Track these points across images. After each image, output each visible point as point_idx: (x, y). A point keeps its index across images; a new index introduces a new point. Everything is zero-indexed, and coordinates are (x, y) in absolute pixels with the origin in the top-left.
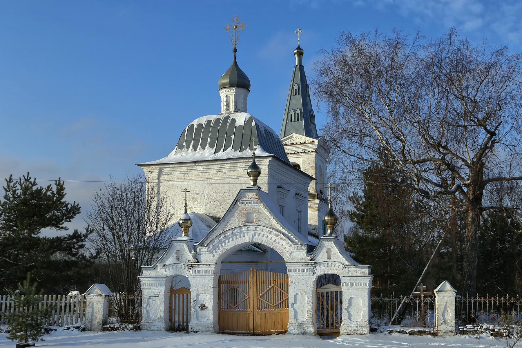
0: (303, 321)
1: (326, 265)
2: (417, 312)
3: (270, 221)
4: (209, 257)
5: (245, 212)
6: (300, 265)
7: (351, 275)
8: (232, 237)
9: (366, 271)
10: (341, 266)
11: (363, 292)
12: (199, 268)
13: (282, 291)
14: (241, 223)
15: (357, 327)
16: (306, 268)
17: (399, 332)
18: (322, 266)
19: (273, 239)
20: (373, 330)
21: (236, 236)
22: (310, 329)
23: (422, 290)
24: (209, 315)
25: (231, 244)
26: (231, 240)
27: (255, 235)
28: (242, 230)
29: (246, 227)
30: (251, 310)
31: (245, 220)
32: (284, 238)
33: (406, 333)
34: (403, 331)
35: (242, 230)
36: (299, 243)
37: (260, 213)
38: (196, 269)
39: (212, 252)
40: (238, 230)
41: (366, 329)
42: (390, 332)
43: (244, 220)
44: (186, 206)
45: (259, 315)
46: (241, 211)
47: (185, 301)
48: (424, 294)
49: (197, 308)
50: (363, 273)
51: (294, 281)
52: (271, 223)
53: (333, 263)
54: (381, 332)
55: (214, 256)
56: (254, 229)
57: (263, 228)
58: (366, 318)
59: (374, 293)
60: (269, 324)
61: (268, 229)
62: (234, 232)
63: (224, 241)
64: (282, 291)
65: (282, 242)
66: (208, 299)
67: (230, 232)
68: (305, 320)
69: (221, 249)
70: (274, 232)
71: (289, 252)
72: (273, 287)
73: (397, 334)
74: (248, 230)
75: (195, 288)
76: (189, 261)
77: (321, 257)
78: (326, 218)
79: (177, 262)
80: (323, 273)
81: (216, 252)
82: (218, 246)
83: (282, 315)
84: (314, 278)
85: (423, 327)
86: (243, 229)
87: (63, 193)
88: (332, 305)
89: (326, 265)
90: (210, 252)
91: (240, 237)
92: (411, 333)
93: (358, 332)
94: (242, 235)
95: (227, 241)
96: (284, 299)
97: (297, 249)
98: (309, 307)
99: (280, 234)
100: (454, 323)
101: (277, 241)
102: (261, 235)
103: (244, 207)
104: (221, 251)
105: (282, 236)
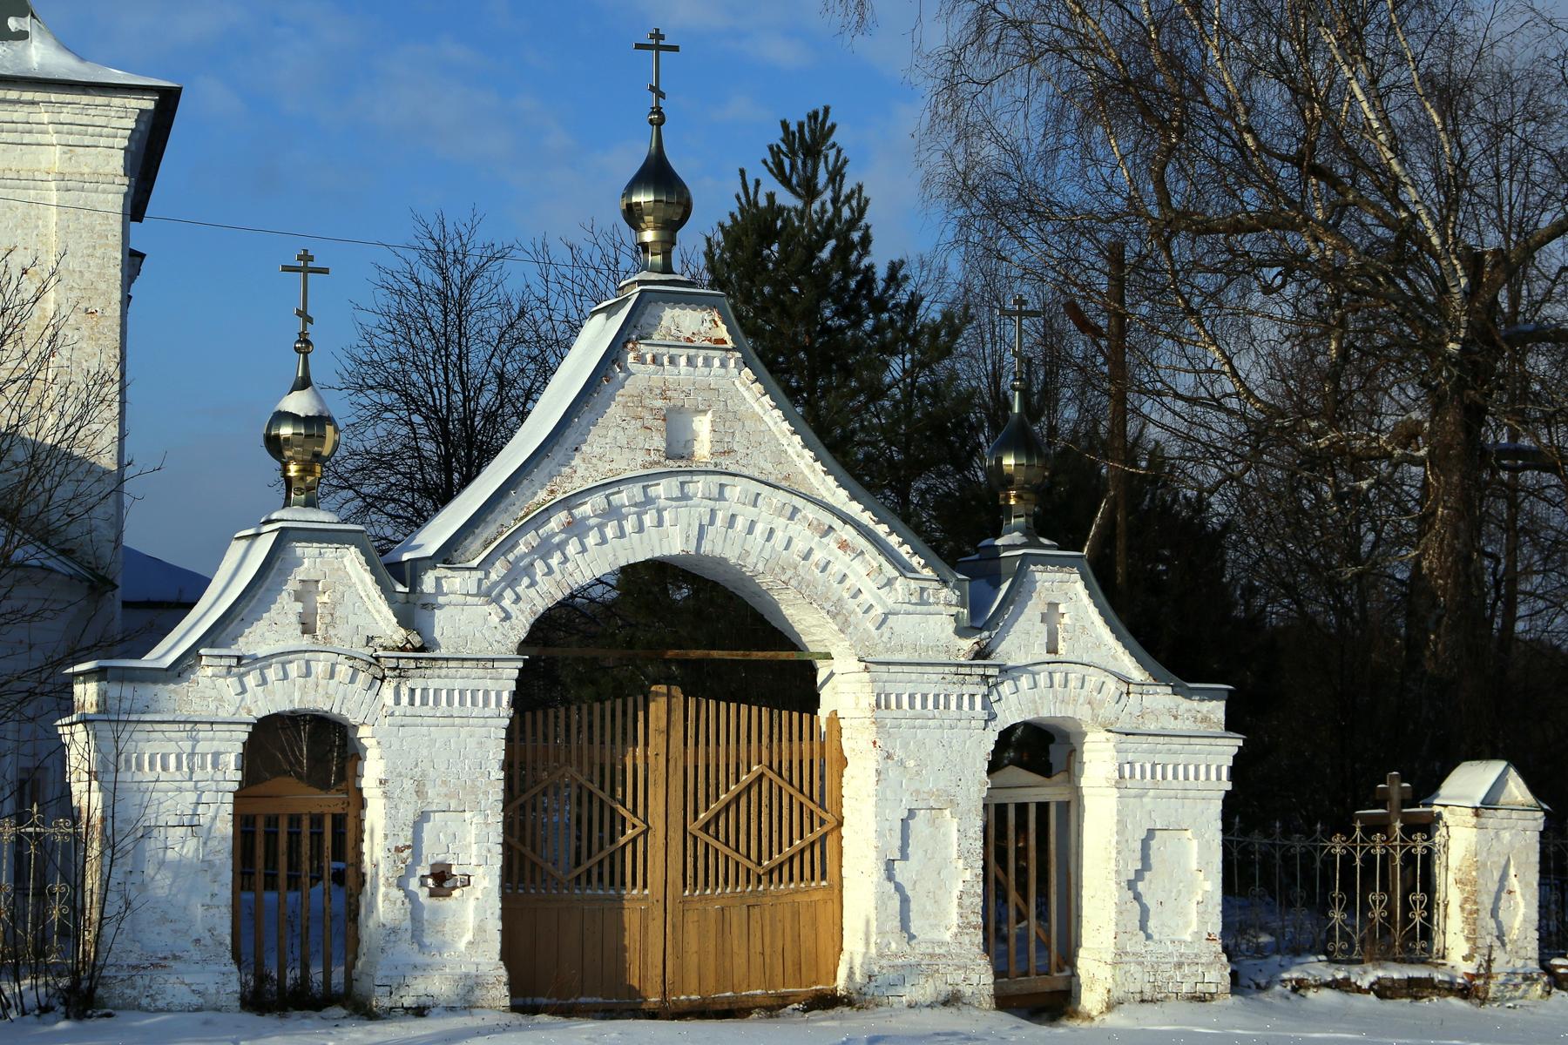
0: (941, 944)
1: (1042, 679)
2: (1375, 896)
3: (780, 456)
4: (483, 623)
5: (659, 403)
6: (933, 674)
7: (1152, 727)
8: (601, 527)
9: (1216, 710)
10: (1112, 685)
11: (1201, 805)
12: (436, 681)
13: (605, 796)
14: (640, 457)
15: (1180, 965)
16: (955, 690)
17: (1328, 985)
18: (1025, 681)
19: (799, 546)
20: (1237, 984)
21: (621, 518)
22: (974, 979)
23: (1396, 797)
24: (472, 926)
25: (588, 563)
26: (592, 539)
27: (712, 522)
28: (652, 491)
29: (674, 482)
30: (654, 889)
31: (662, 445)
32: (862, 543)
33: (1359, 990)
34: (1347, 980)
35: (652, 491)
36: (928, 572)
37: (728, 419)
38: (418, 684)
39: (497, 600)
40: (636, 490)
41: (1217, 975)
42: (1299, 986)
43: (658, 442)
44: (305, 345)
45: (692, 917)
46: (641, 396)
47: (690, 860)
48: (1404, 818)
49: (414, 884)
50: (1205, 719)
51: (899, 753)
52: (787, 470)
53: (1075, 673)
54: (1258, 987)
55: (507, 617)
56: (715, 492)
57: (755, 487)
58: (1215, 925)
59: (1242, 811)
60: (740, 961)
61: (780, 497)
62: (615, 499)
63: (561, 546)
64: (797, 796)
65: (841, 563)
66: (475, 843)
67: (598, 500)
68: (947, 937)
69: (544, 584)
70: (811, 512)
71: (878, 610)
72: (761, 776)
73: (1326, 994)
74: (684, 497)
75: (408, 784)
76: (370, 639)
77: (1020, 641)
78: (1009, 461)
79: (306, 642)
80: (1028, 716)
81: (518, 599)
82: (529, 570)
83: (796, 914)
84: (991, 738)
85: (1403, 961)
86: (661, 489)
87: (868, 276)
88: (1022, 872)
89: (1042, 679)
90: (490, 595)
91: (641, 529)
92: (1383, 990)
93: (1185, 988)
94: (648, 519)
95: (572, 548)
96: (808, 836)
97: (922, 602)
98: (968, 875)
99: (837, 524)
100: (1535, 944)
101: (818, 556)
102: (740, 523)
103: (656, 380)
104: (542, 593)
105: (848, 533)
